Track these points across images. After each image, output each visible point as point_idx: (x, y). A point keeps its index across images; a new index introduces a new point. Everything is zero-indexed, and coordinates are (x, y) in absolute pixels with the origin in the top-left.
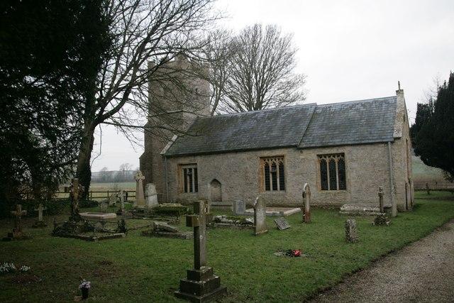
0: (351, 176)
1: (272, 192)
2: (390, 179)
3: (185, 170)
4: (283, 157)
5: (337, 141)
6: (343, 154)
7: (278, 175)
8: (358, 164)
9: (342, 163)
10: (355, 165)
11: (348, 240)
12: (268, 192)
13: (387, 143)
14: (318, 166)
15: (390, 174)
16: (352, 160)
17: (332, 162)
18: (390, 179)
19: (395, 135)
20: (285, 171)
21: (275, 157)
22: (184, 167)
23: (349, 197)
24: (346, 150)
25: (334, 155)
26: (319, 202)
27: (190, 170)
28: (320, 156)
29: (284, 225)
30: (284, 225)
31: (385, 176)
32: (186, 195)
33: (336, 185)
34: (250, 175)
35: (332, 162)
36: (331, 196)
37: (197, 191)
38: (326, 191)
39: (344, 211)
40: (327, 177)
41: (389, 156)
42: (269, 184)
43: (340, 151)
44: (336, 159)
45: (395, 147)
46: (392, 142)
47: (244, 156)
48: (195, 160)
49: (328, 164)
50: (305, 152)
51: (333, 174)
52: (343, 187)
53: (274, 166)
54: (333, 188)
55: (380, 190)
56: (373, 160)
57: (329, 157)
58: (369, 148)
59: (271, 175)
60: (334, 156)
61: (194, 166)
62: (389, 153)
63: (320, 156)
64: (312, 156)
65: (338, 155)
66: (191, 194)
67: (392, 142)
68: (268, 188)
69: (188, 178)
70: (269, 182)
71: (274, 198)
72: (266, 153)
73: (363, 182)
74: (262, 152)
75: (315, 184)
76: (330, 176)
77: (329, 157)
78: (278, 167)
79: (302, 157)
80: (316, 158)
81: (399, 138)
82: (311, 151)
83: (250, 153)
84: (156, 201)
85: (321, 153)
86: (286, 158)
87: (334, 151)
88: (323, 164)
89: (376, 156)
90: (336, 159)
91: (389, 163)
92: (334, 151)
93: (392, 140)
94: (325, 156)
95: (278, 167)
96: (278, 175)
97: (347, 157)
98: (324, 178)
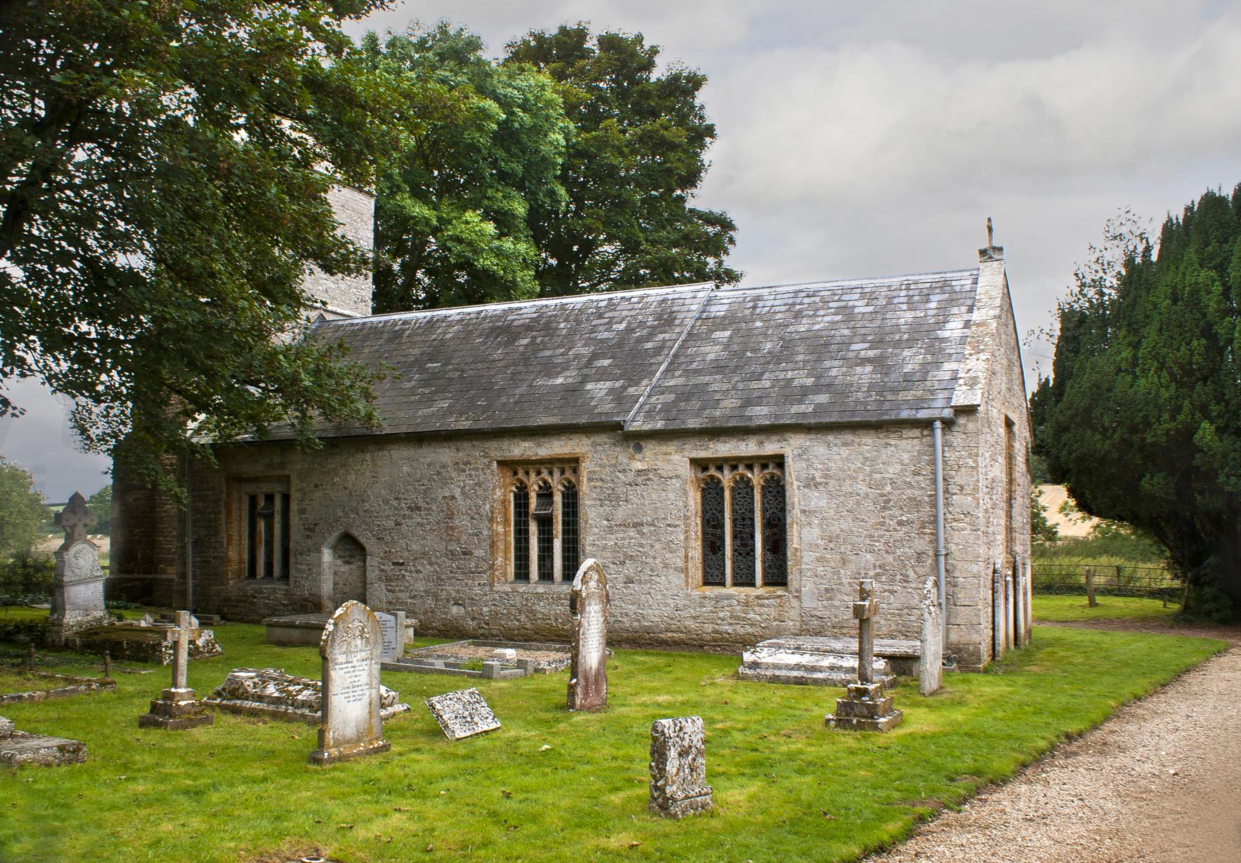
0: (802, 537)
1: (535, 585)
2: (937, 555)
3: (253, 500)
4: (573, 463)
5: (761, 414)
6: (779, 461)
7: (558, 528)
8: (832, 493)
9: (776, 491)
10: (818, 500)
11: (661, 804)
12: (522, 588)
13: (928, 424)
14: (694, 499)
15: (935, 535)
16: (811, 483)
17: (743, 487)
18: (937, 555)
19: (961, 397)
20: (787, 494)
21: (550, 462)
22: (251, 488)
23: (793, 614)
24: (790, 447)
25: (750, 463)
26: (692, 624)
27: (270, 498)
28: (700, 464)
29: (468, 721)
30: (468, 721)
31: (921, 544)
32: (250, 587)
33: (723, 574)
34: (462, 522)
35: (743, 487)
36: (735, 604)
37: (285, 576)
38: (718, 590)
39: (755, 665)
40: (722, 538)
41: (934, 473)
42: (527, 558)
43: (771, 447)
44: (756, 478)
45: (957, 438)
46: (948, 424)
47: (445, 455)
48: (283, 465)
49: (727, 494)
50: (651, 450)
51: (747, 531)
52: (778, 576)
53: (546, 495)
54: (744, 579)
55: (864, 594)
56: (880, 485)
57: (734, 468)
58: (868, 442)
59: (533, 528)
60: (720, 469)
61: (277, 489)
62: (933, 463)
63: (700, 464)
64: (676, 460)
65: (764, 462)
66: (267, 587)
67: (948, 424)
68: (522, 573)
69: (262, 525)
70: (527, 549)
71: (541, 607)
72: (724, 449)
73: (844, 562)
74: (505, 444)
75: (680, 563)
76: (735, 537)
77: (734, 468)
78: (558, 498)
79: (638, 465)
80: (686, 471)
81: (970, 410)
82: (671, 447)
83: (466, 445)
84: (101, 602)
85: (703, 454)
86: (586, 467)
87: (748, 448)
88: (711, 492)
89: (893, 470)
90: (756, 478)
91: (934, 497)
92: (748, 448)
93: (948, 413)
94: (720, 464)
95: (558, 498)
96: (558, 528)
97: (794, 471)
98: (712, 546)
